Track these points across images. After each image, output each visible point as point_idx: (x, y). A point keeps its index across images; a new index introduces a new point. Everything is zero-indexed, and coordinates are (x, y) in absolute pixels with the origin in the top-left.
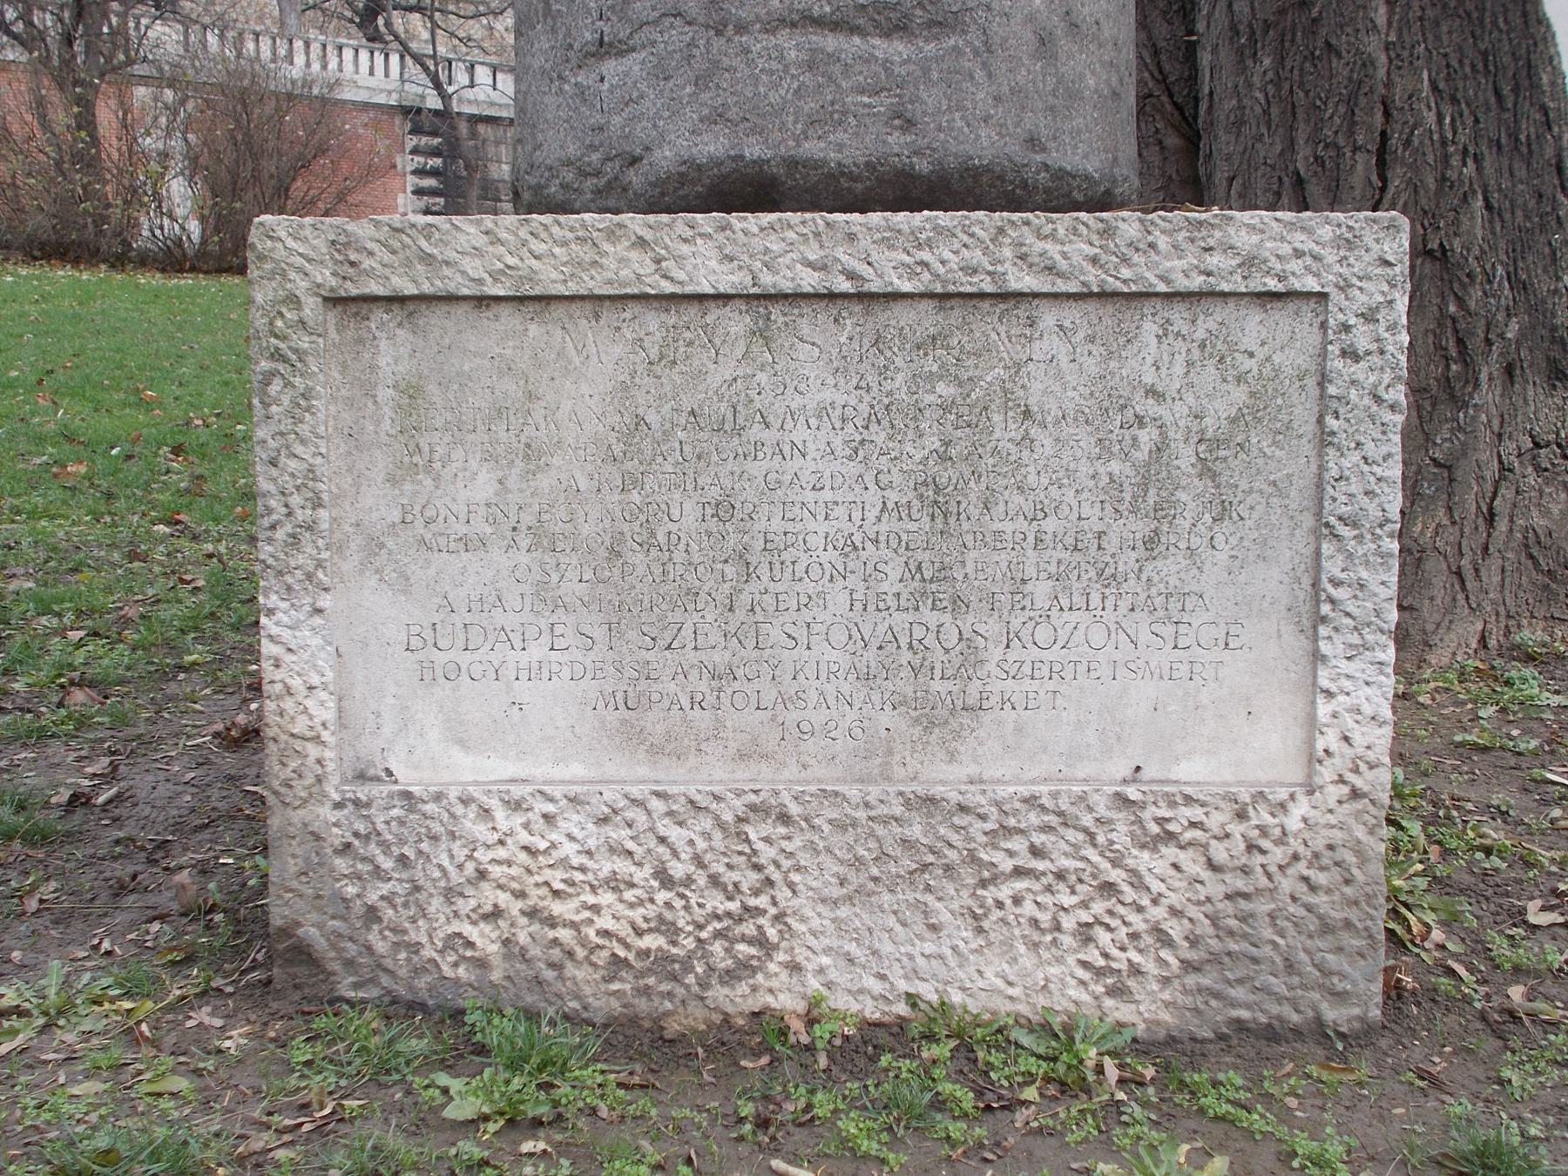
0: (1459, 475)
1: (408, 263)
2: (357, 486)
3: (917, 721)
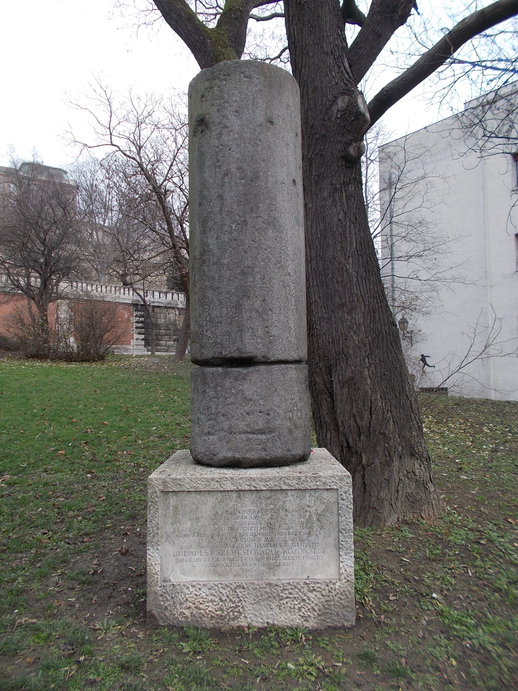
0: (390, 481)
1: (176, 485)
2: (165, 525)
3: (268, 568)
